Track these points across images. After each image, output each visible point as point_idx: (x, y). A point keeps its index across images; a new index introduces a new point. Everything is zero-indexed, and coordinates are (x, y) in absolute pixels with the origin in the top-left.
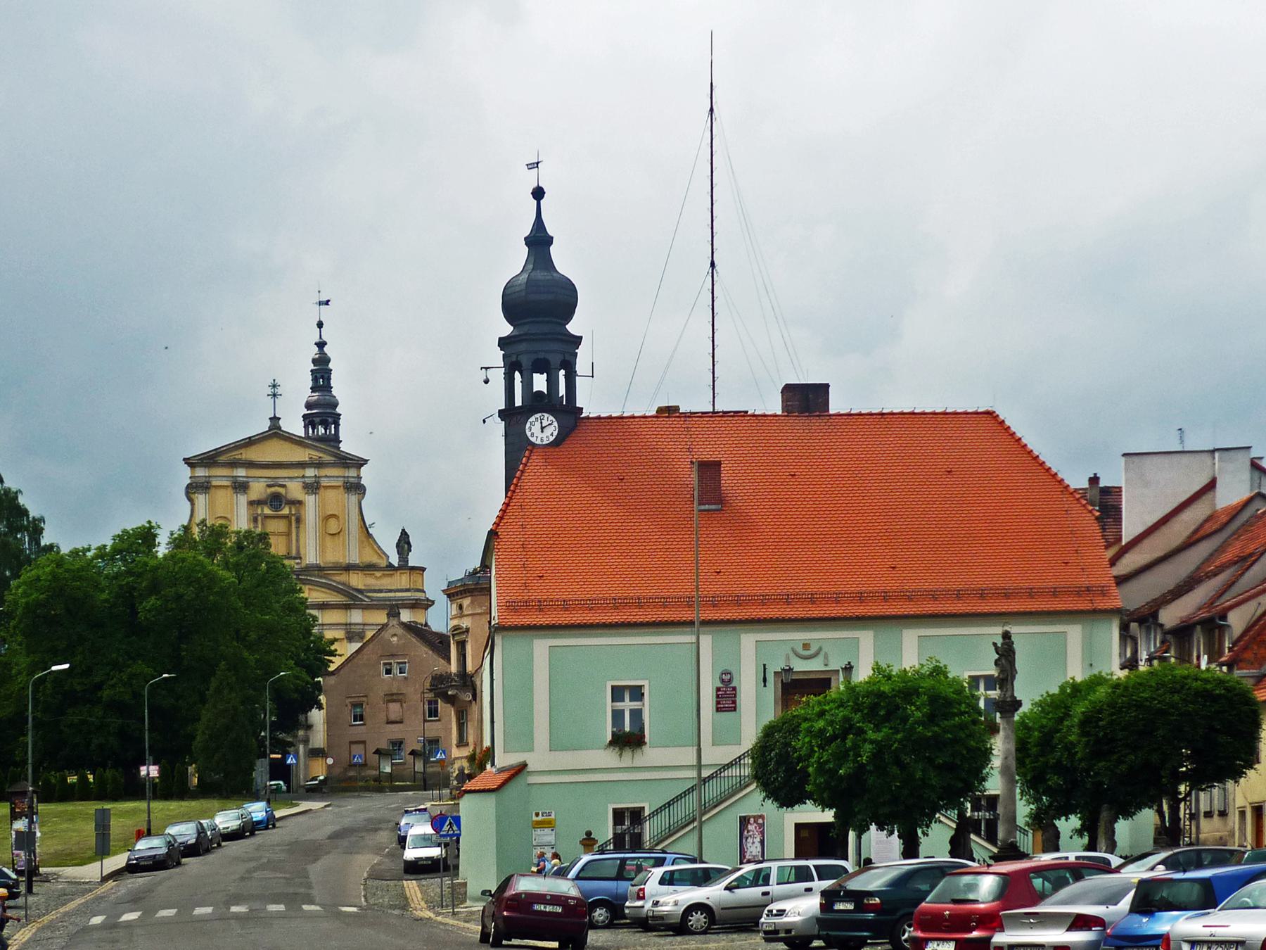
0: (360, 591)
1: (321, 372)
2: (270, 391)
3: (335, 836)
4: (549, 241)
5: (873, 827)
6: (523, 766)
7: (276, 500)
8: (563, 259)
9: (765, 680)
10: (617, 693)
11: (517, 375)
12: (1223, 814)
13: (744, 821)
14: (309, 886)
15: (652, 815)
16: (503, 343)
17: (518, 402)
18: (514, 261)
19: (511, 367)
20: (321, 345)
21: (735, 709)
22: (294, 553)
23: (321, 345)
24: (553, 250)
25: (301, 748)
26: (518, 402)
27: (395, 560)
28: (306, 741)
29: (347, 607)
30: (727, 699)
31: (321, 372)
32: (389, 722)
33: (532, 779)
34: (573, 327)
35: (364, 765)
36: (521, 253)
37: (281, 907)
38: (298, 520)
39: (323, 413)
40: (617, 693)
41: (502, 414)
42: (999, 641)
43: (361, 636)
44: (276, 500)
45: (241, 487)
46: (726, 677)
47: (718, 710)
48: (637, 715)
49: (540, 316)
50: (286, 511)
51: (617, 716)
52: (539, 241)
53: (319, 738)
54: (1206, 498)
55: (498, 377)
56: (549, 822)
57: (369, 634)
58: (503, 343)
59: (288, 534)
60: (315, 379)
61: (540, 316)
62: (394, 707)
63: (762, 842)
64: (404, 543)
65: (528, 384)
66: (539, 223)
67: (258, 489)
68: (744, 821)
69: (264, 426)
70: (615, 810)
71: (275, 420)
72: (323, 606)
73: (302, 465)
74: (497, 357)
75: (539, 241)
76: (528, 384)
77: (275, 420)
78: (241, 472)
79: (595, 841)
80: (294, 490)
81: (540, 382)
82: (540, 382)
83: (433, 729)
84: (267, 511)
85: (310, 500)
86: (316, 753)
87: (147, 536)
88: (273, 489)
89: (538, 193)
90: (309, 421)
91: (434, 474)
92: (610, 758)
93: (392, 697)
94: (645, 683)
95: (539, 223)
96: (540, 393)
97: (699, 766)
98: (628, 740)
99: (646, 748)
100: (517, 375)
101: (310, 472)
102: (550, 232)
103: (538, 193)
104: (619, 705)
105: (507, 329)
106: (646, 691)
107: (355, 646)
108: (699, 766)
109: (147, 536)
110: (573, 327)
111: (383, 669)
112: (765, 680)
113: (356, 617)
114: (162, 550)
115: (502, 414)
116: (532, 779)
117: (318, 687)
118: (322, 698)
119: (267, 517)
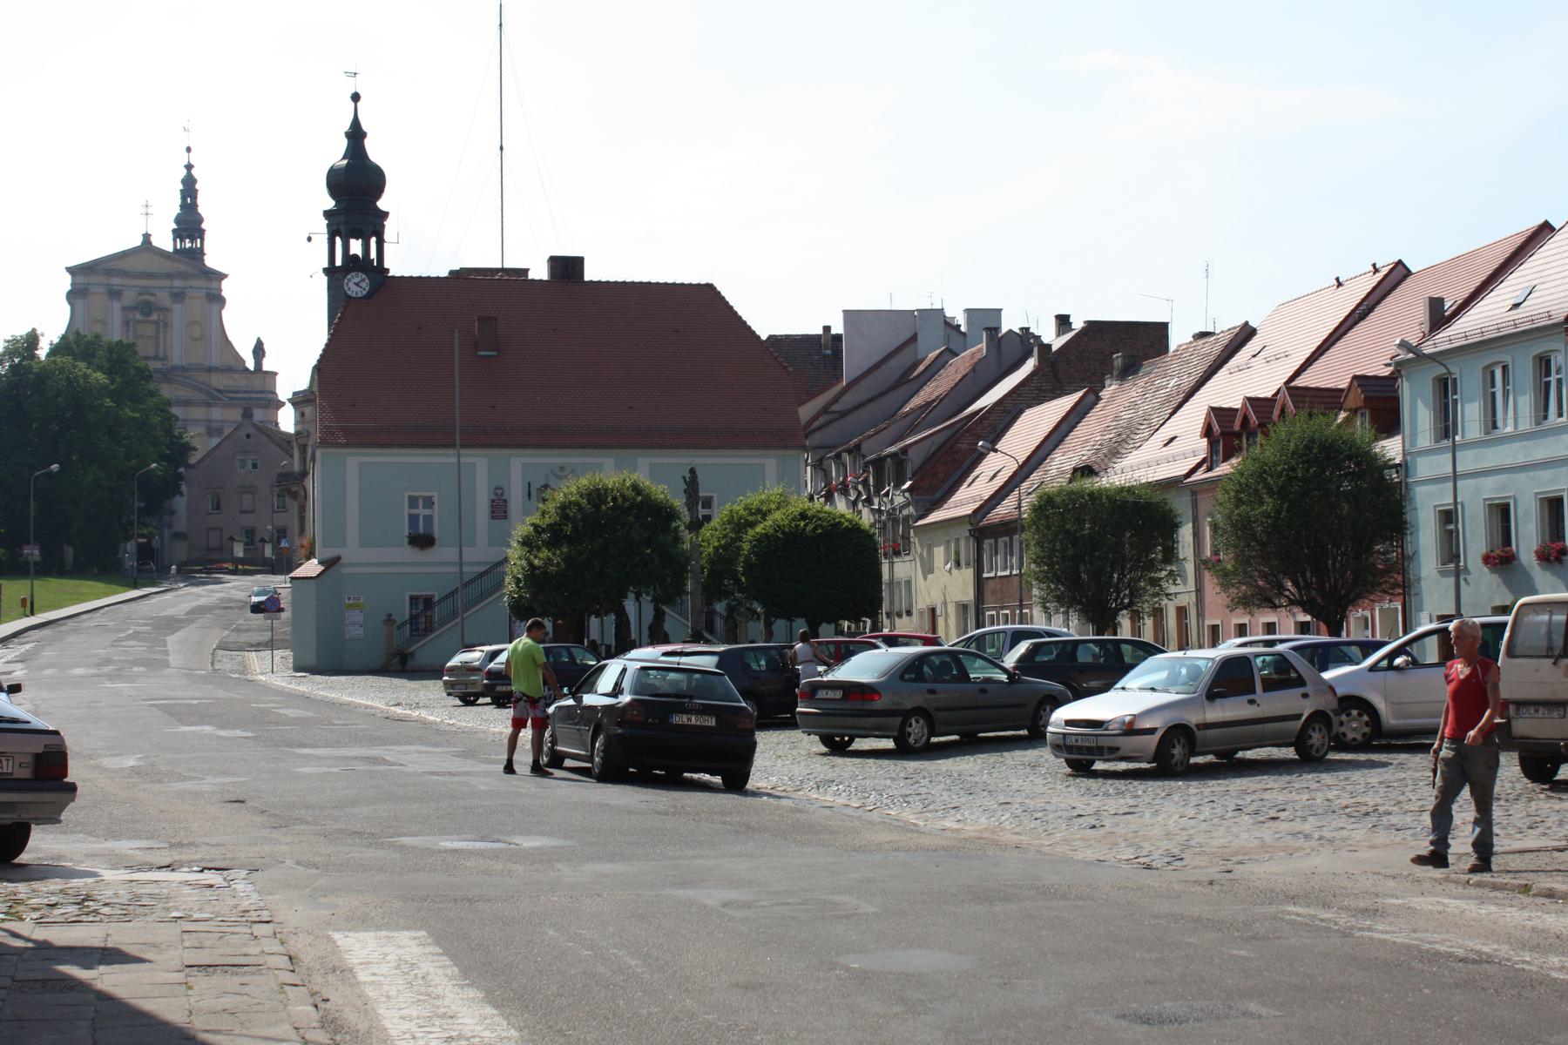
0: (220, 391)
1: (189, 188)
2: (144, 210)
3: (193, 612)
4: (364, 135)
6: (338, 559)
7: (147, 308)
8: (374, 150)
10: (413, 501)
11: (338, 240)
12: (909, 613)
14: (166, 653)
15: (440, 601)
16: (327, 214)
17: (339, 262)
18: (335, 152)
19: (332, 234)
20: (189, 167)
22: (161, 354)
23: (189, 167)
24: (367, 142)
25: (166, 531)
26: (339, 262)
27: (250, 365)
28: (170, 526)
29: (208, 405)
30: (499, 509)
31: (189, 188)
32: (242, 512)
33: (344, 570)
34: (382, 204)
35: (221, 549)
36: (343, 144)
37: (142, 669)
38: (166, 325)
39: (189, 224)
40: (413, 501)
41: (326, 271)
42: (688, 475)
43: (220, 431)
44: (147, 308)
45: (115, 294)
46: (421, 511)
48: (428, 519)
49: (356, 193)
50: (154, 317)
51: (413, 519)
52: (356, 135)
53: (181, 523)
54: (910, 348)
56: (358, 606)
57: (227, 431)
58: (327, 214)
59: (157, 338)
60: (184, 198)
61: (356, 193)
62: (247, 498)
64: (259, 351)
65: (346, 247)
66: (356, 123)
67: (130, 297)
69: (138, 242)
70: (412, 598)
71: (147, 237)
72: (187, 403)
73: (170, 276)
74: (322, 224)
75: (356, 135)
76: (346, 247)
77: (147, 237)
78: (116, 281)
79: (394, 621)
80: (164, 298)
81: (356, 247)
82: (356, 247)
83: (281, 519)
84: (138, 316)
85: (176, 307)
86: (179, 536)
87: (32, 339)
88: (141, 298)
89: (356, 97)
90: (178, 234)
91: (278, 319)
93: (249, 490)
94: (435, 494)
95: (356, 123)
96: (355, 256)
97: (461, 564)
98: (422, 541)
99: (436, 547)
100: (338, 240)
101: (177, 283)
103: (356, 97)
104: (428, 512)
105: (330, 204)
106: (435, 500)
107: (215, 441)
108: (461, 564)
109: (32, 339)
110: (382, 204)
111: (238, 464)
113: (217, 414)
114: (42, 352)
115: (326, 271)
116: (344, 570)
117: (180, 477)
118: (184, 488)
119: (138, 322)
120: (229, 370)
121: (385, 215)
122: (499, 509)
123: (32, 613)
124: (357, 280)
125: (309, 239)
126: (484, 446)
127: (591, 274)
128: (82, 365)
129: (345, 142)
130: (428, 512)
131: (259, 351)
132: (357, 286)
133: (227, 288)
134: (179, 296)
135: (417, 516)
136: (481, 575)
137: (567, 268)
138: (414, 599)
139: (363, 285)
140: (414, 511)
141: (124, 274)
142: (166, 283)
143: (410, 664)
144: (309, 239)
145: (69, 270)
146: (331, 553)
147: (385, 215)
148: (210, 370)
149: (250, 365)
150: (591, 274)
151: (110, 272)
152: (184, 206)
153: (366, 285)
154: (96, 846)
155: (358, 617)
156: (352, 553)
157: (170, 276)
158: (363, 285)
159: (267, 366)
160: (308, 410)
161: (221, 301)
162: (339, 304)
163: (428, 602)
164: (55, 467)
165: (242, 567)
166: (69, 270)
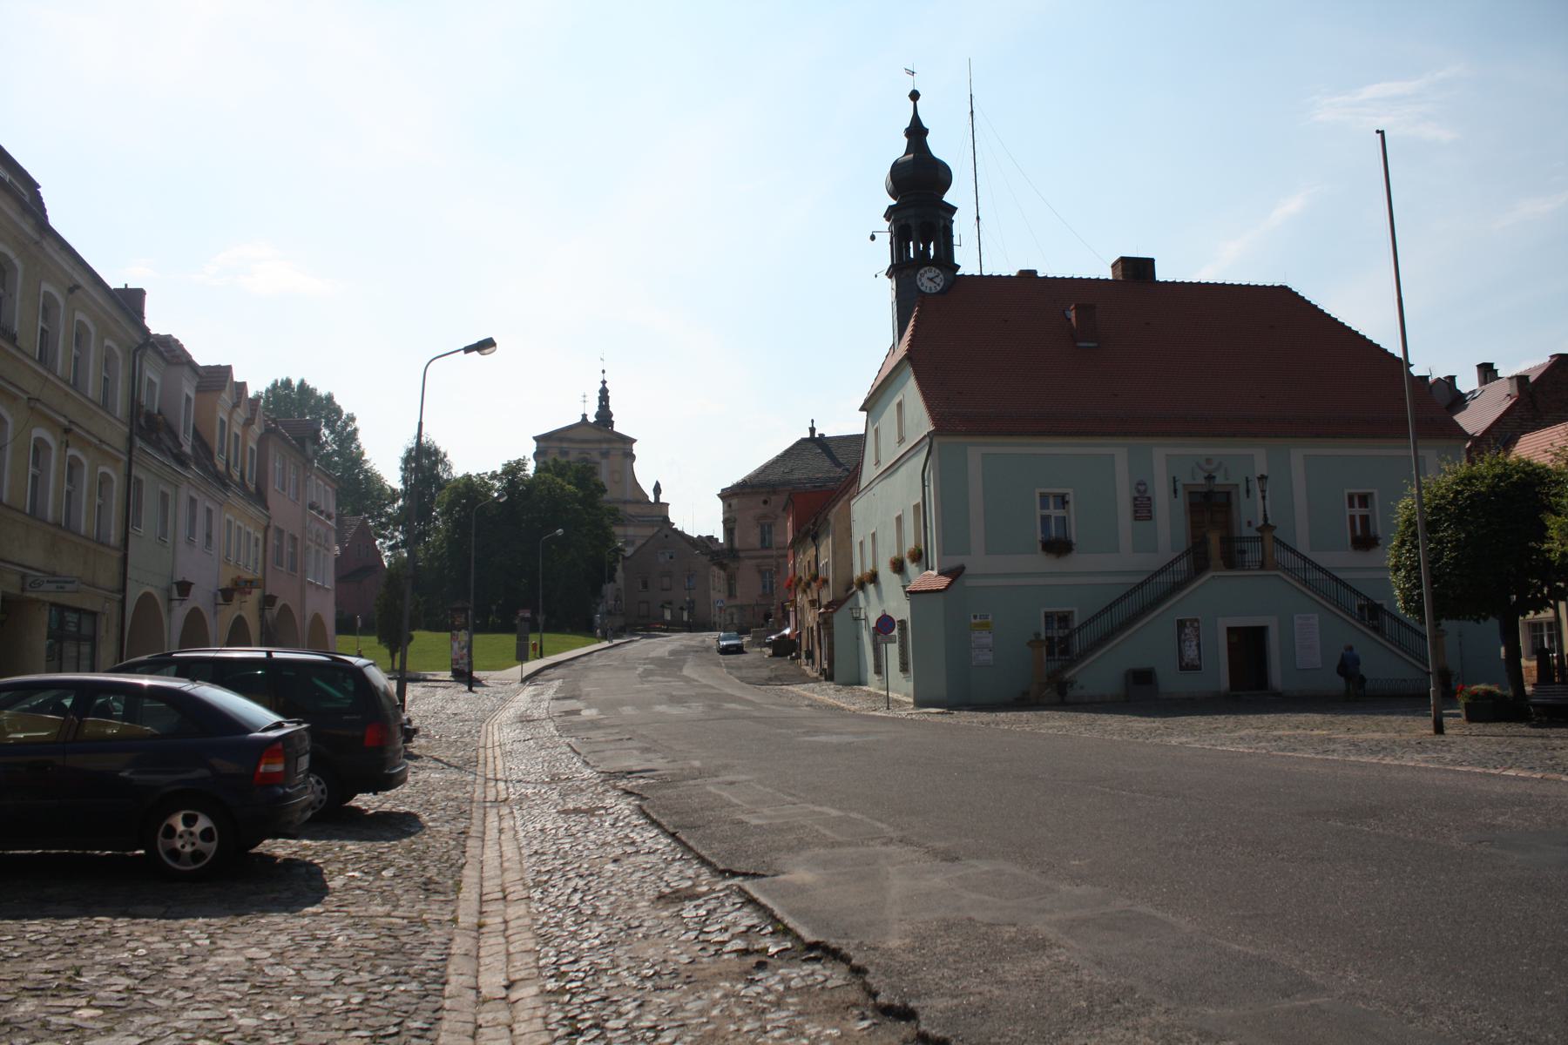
1: (604, 395)
5: (720, 535)
8: (938, 146)
9: (1175, 491)
13: (1181, 624)
18: (898, 147)
20: (604, 382)
21: (1150, 518)
23: (604, 382)
24: (928, 139)
27: (652, 499)
31: (604, 395)
33: (969, 582)
34: (948, 198)
39: (605, 415)
46: (1142, 488)
47: (1136, 518)
48: (1063, 521)
49: (920, 194)
51: (1045, 520)
52: (916, 132)
55: (885, 240)
61: (920, 194)
63: (1198, 645)
64: (657, 489)
66: (916, 118)
68: (1181, 624)
69: (578, 419)
71: (584, 416)
73: (599, 441)
75: (916, 132)
78: (565, 445)
80: (595, 456)
85: (604, 462)
89: (915, 96)
92: (1041, 562)
94: (1070, 491)
95: (916, 118)
98: (1058, 546)
101: (605, 446)
102: (926, 125)
103: (915, 96)
104: (1364, 511)
106: (1070, 498)
110: (948, 198)
112: (1175, 491)
116: (969, 582)
120: (638, 502)
121: (953, 210)
122: (1143, 508)
123: (541, 656)
124: (931, 275)
125: (873, 238)
126: (1126, 434)
127: (1162, 274)
128: (559, 480)
129: (905, 140)
130: (1060, 513)
131: (657, 489)
132: (929, 281)
133: (636, 448)
134: (605, 454)
135: (1049, 517)
136: (1142, 584)
137: (1136, 270)
138: (1048, 616)
139: (938, 280)
140: (1046, 512)
141: (571, 440)
142: (597, 446)
143: (1072, 694)
144: (873, 238)
145: (535, 438)
146: (955, 561)
147: (953, 210)
148: (625, 502)
149: (652, 499)
150: (1162, 274)
151: (561, 440)
152: (601, 406)
153: (940, 280)
154: (115, 484)
155: (986, 638)
156: (977, 562)
157: (599, 441)
158: (938, 280)
159: (662, 499)
160: (734, 502)
161: (633, 457)
162: (907, 302)
163: (1064, 619)
164: (560, 531)
165: (675, 626)
166: (535, 438)
